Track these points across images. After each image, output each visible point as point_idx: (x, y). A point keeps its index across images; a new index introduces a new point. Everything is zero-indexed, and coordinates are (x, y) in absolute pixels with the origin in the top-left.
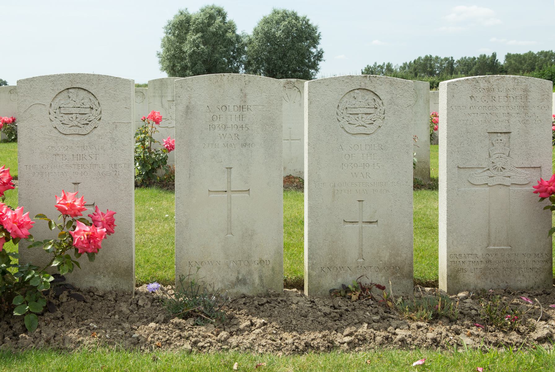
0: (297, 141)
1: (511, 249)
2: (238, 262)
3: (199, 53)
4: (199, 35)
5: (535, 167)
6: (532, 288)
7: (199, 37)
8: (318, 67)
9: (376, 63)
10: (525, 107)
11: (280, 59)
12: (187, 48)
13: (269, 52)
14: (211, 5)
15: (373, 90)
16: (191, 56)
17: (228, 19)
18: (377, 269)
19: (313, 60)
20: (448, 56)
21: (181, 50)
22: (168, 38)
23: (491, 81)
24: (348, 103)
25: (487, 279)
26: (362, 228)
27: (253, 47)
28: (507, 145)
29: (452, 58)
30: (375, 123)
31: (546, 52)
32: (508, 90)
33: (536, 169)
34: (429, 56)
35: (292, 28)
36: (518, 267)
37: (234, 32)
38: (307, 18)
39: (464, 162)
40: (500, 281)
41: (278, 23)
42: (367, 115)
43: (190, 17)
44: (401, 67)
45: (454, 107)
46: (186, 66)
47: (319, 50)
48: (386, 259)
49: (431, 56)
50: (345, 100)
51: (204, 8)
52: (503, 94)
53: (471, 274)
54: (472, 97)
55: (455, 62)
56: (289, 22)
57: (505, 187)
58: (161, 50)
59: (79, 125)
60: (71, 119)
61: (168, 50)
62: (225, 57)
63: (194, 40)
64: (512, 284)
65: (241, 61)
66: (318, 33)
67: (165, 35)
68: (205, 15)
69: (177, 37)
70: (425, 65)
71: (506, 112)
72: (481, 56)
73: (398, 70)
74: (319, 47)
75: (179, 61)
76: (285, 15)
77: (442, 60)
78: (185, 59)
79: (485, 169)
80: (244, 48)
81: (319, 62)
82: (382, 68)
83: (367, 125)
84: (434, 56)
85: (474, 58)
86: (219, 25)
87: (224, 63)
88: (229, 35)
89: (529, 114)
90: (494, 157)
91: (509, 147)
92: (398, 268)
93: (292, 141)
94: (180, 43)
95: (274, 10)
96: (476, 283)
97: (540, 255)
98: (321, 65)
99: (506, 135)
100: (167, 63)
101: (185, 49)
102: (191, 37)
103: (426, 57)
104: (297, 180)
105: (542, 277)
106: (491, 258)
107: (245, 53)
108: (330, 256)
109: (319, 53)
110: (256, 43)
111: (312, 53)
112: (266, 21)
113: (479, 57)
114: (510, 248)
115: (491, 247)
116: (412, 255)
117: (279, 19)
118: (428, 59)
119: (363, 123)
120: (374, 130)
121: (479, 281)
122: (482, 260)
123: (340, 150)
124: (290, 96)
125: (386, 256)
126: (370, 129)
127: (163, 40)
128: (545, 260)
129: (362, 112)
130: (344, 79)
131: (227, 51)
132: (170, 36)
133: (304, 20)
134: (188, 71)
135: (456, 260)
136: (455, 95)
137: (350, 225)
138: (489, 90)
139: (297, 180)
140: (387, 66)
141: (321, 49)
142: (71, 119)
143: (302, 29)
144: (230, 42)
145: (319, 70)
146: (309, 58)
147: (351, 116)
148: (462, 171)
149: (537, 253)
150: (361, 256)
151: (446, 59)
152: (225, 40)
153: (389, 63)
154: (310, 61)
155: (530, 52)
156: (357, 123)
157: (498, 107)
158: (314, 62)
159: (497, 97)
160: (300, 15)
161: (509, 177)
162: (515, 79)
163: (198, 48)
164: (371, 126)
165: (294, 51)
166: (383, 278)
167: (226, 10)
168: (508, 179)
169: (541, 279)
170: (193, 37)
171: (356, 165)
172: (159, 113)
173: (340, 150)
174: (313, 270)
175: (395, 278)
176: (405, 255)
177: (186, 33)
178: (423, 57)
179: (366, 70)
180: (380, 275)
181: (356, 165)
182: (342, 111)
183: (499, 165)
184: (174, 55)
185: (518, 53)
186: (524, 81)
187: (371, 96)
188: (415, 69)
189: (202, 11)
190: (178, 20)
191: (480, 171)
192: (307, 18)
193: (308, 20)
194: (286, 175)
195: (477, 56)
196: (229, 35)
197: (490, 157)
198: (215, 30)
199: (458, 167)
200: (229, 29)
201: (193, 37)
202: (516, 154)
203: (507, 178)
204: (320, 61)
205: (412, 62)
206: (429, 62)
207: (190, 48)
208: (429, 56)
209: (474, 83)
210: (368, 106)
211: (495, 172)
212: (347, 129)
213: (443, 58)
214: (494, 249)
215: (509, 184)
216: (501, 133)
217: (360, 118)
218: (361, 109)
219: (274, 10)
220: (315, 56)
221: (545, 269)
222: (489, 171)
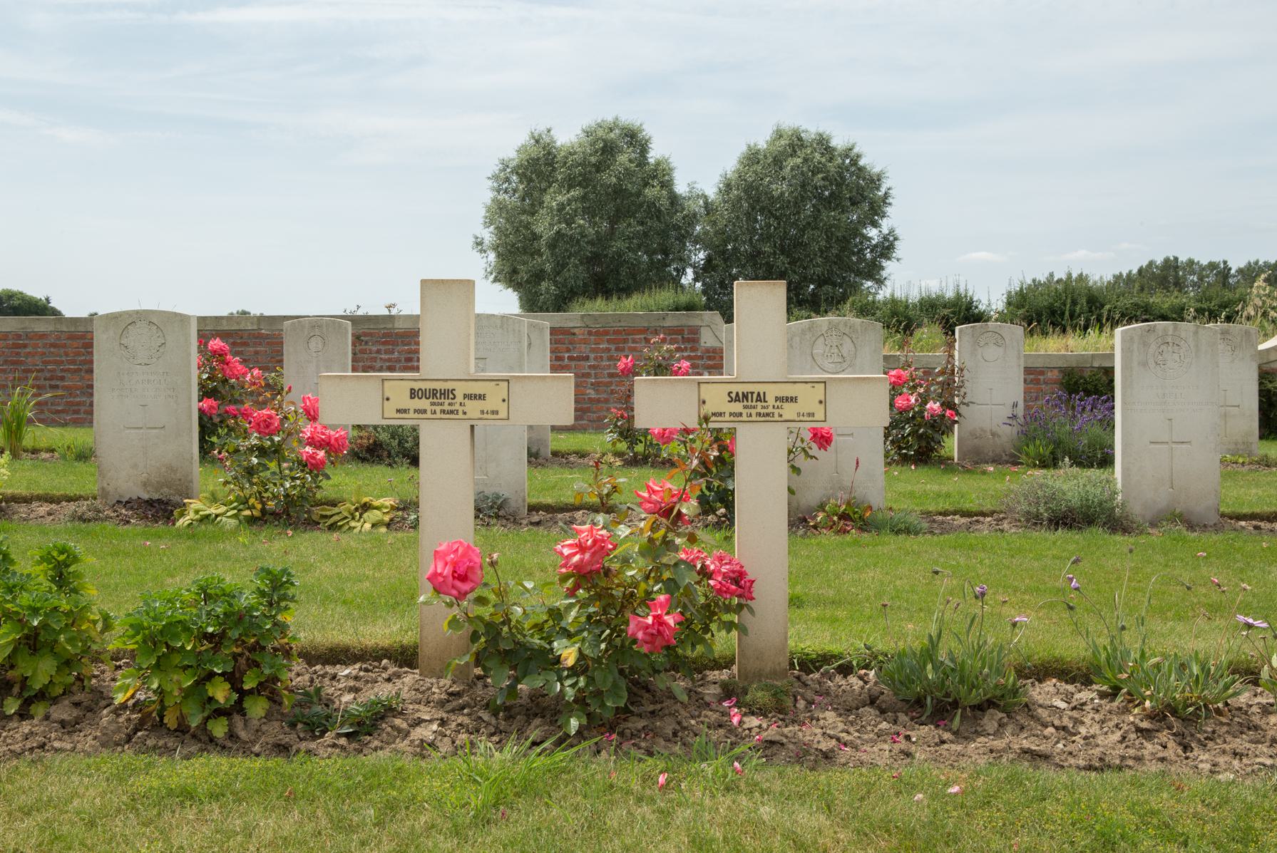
3: (571, 237)
8: (884, 274)
9: (1052, 275)
12: (544, 226)
14: (610, 118)
16: (552, 245)
17: (653, 155)
20: (1216, 259)
29: (1225, 262)
35: (813, 174)
38: (855, 151)
46: (542, 271)
47: (885, 231)
49: (1176, 259)
55: (1233, 272)
56: (806, 160)
58: (488, 235)
63: (561, 207)
66: (883, 190)
74: (885, 225)
76: (796, 143)
77: (1203, 269)
81: (885, 263)
84: (1183, 258)
86: (626, 169)
98: (890, 268)
102: (555, 198)
103: (1167, 260)
110: (724, 214)
111: (869, 239)
112: (752, 158)
117: (782, 153)
118: (1171, 265)
131: (645, 234)
141: (891, 231)
144: (654, 211)
145: (887, 282)
146: (861, 251)
151: (1212, 266)
158: (874, 260)
160: (838, 142)
165: (816, 233)
167: (649, 130)
170: (559, 198)
178: (1159, 260)
192: (855, 151)
193: (859, 156)
198: (614, 180)
200: (655, 177)
201: (559, 198)
204: (889, 259)
205: (1135, 271)
207: (551, 225)
213: (1204, 262)
220: (876, 246)
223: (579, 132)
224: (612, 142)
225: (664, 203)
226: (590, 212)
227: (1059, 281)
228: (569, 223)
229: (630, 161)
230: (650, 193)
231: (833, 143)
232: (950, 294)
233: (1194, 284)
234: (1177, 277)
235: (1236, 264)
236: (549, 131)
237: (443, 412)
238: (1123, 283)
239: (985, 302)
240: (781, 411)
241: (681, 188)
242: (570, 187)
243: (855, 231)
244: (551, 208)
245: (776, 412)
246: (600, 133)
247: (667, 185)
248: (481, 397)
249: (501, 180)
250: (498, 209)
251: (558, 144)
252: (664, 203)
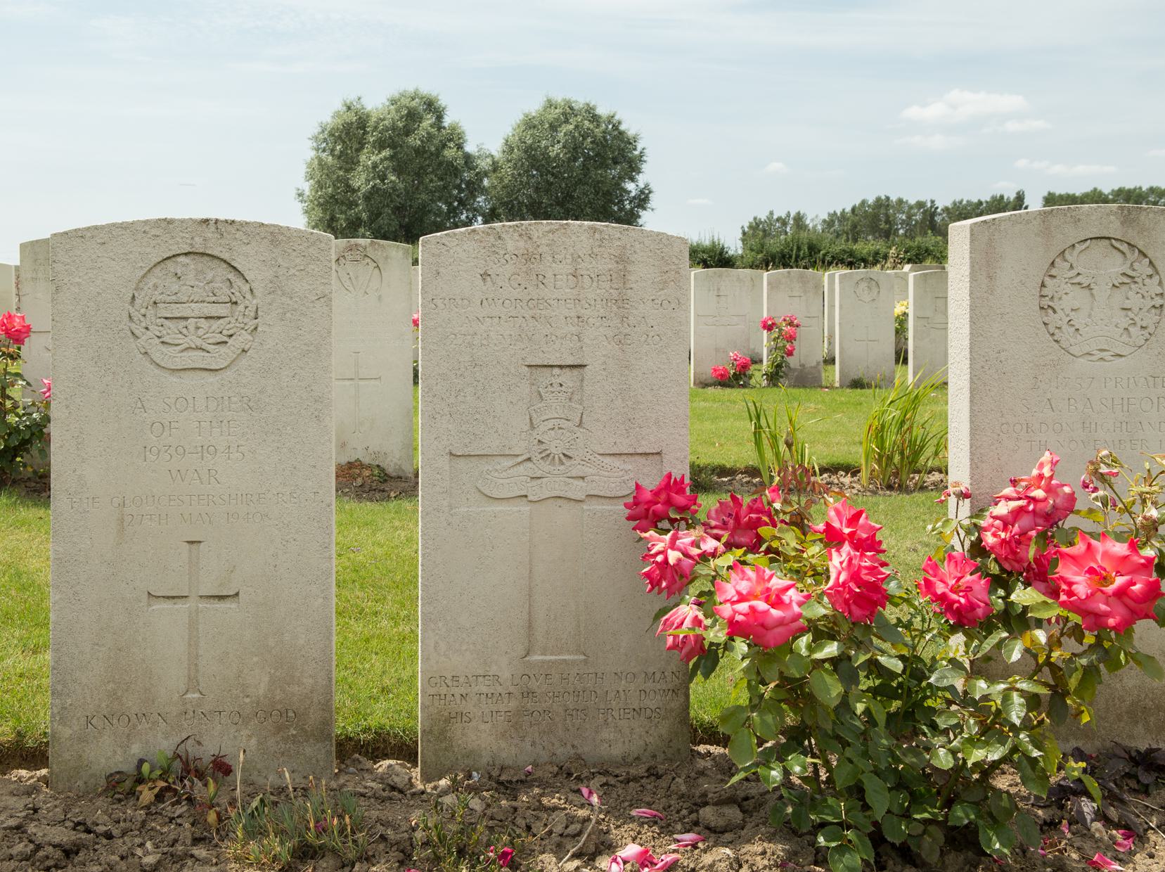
0: (372, 382)
1: (586, 662)
3: (385, 192)
4: (386, 153)
5: (646, 454)
6: (638, 758)
7: (386, 159)
9: (771, 213)
10: (621, 301)
11: (558, 204)
12: (360, 181)
13: (537, 189)
14: (411, 89)
15: (226, 256)
16: (368, 198)
17: (447, 121)
18: (236, 719)
19: (628, 207)
20: (923, 199)
21: (348, 186)
22: (320, 160)
23: (535, 235)
24: (160, 290)
25: (523, 739)
26: (197, 611)
27: (501, 179)
28: (576, 397)
29: (933, 202)
30: (231, 341)
31: (1129, 191)
32: (576, 258)
33: (651, 457)
35: (584, 139)
36: (602, 706)
37: (460, 147)
38: (617, 118)
39: (467, 441)
40: (557, 744)
41: (553, 127)
42: (212, 321)
43: (368, 116)
44: (824, 221)
45: (439, 302)
46: (359, 219)
47: (642, 185)
48: (261, 692)
49: (888, 198)
50: (152, 280)
51: (397, 95)
52: (565, 268)
53: (483, 727)
54: (485, 276)
56: (577, 127)
57: (572, 503)
58: (307, 187)
59: (205, 346)
60: (184, 331)
61: (320, 185)
62: (440, 199)
63: (375, 166)
64: (586, 749)
65: (475, 210)
67: (313, 153)
68: (398, 111)
69: (339, 157)
70: (875, 217)
71: (573, 314)
73: (819, 227)
74: (642, 179)
75: (344, 208)
76: (569, 112)
77: (911, 207)
78: (357, 205)
79: (520, 459)
80: (481, 181)
81: (642, 213)
82: (784, 223)
83: (210, 348)
87: (439, 213)
88: (449, 153)
89: (632, 320)
90: (543, 428)
91: (581, 402)
92: (291, 714)
93: (361, 383)
94: (347, 171)
95: (549, 101)
96: (494, 748)
97: (658, 676)
99: (576, 372)
100: (319, 213)
101: (356, 183)
102: (369, 158)
103: (878, 199)
104: (367, 473)
105: (664, 729)
106: (534, 685)
107: (484, 191)
108: (111, 685)
110: (507, 170)
112: (530, 124)
114: (582, 657)
115: (537, 657)
116: (330, 679)
117: (557, 120)
118: (882, 204)
119: (199, 342)
120: (229, 361)
121: (503, 745)
122: (511, 689)
123: (137, 411)
124: (357, 277)
125: (260, 683)
126: (220, 357)
127: (310, 165)
128: (670, 686)
129: (197, 313)
130: (147, 228)
131: (445, 187)
132: (324, 155)
133: (609, 122)
134: (362, 230)
135: (444, 690)
136: (441, 270)
137: (167, 605)
138: (529, 258)
139: (367, 473)
140: (795, 219)
141: (647, 186)
142: (184, 331)
143: (606, 141)
144: (452, 170)
146: (621, 201)
147: (166, 322)
148: (462, 463)
149: (651, 670)
150: (193, 683)
151: (920, 205)
152: (440, 164)
153: (799, 213)
154: (621, 210)
155: (1095, 189)
156: (185, 342)
157: (552, 302)
158: (632, 209)
159: (549, 275)
160: (602, 111)
161: (583, 478)
162: (595, 230)
163: (382, 181)
164: (223, 349)
165: (587, 188)
166: (253, 741)
167: (442, 101)
168: (580, 483)
169: (660, 736)
170: (373, 158)
171: (180, 450)
172: (23, 318)
173: (137, 411)
174: (65, 725)
175: (286, 740)
176: (311, 681)
177: (359, 150)
178: (871, 201)
179: (750, 227)
180: (245, 732)
181: (180, 450)
182: (143, 311)
183: (556, 448)
184: (332, 197)
185: (1071, 192)
186: (618, 235)
187: (223, 271)
188: (854, 226)
189: (393, 102)
190: (340, 121)
191: (507, 463)
193: (620, 123)
194: (344, 460)
196: (449, 153)
197: (532, 427)
199: (451, 454)
200: (450, 140)
201: (373, 158)
202: (598, 420)
203: (576, 482)
204: (645, 209)
205: (848, 209)
206: (883, 211)
207: (368, 181)
209: (492, 239)
210: (214, 299)
211: (546, 466)
212: (156, 357)
213: (912, 202)
214: (543, 662)
215: (581, 496)
216: (561, 367)
217: (192, 328)
218: (193, 305)
219: (549, 101)
220: (634, 198)
221: (672, 710)
222: (529, 465)
224: (415, 109)
226: (399, 171)
232: (707, 243)
233: (903, 222)
234: (887, 216)
235: (941, 204)
239: (733, 248)
243: (617, 185)
246: (405, 102)
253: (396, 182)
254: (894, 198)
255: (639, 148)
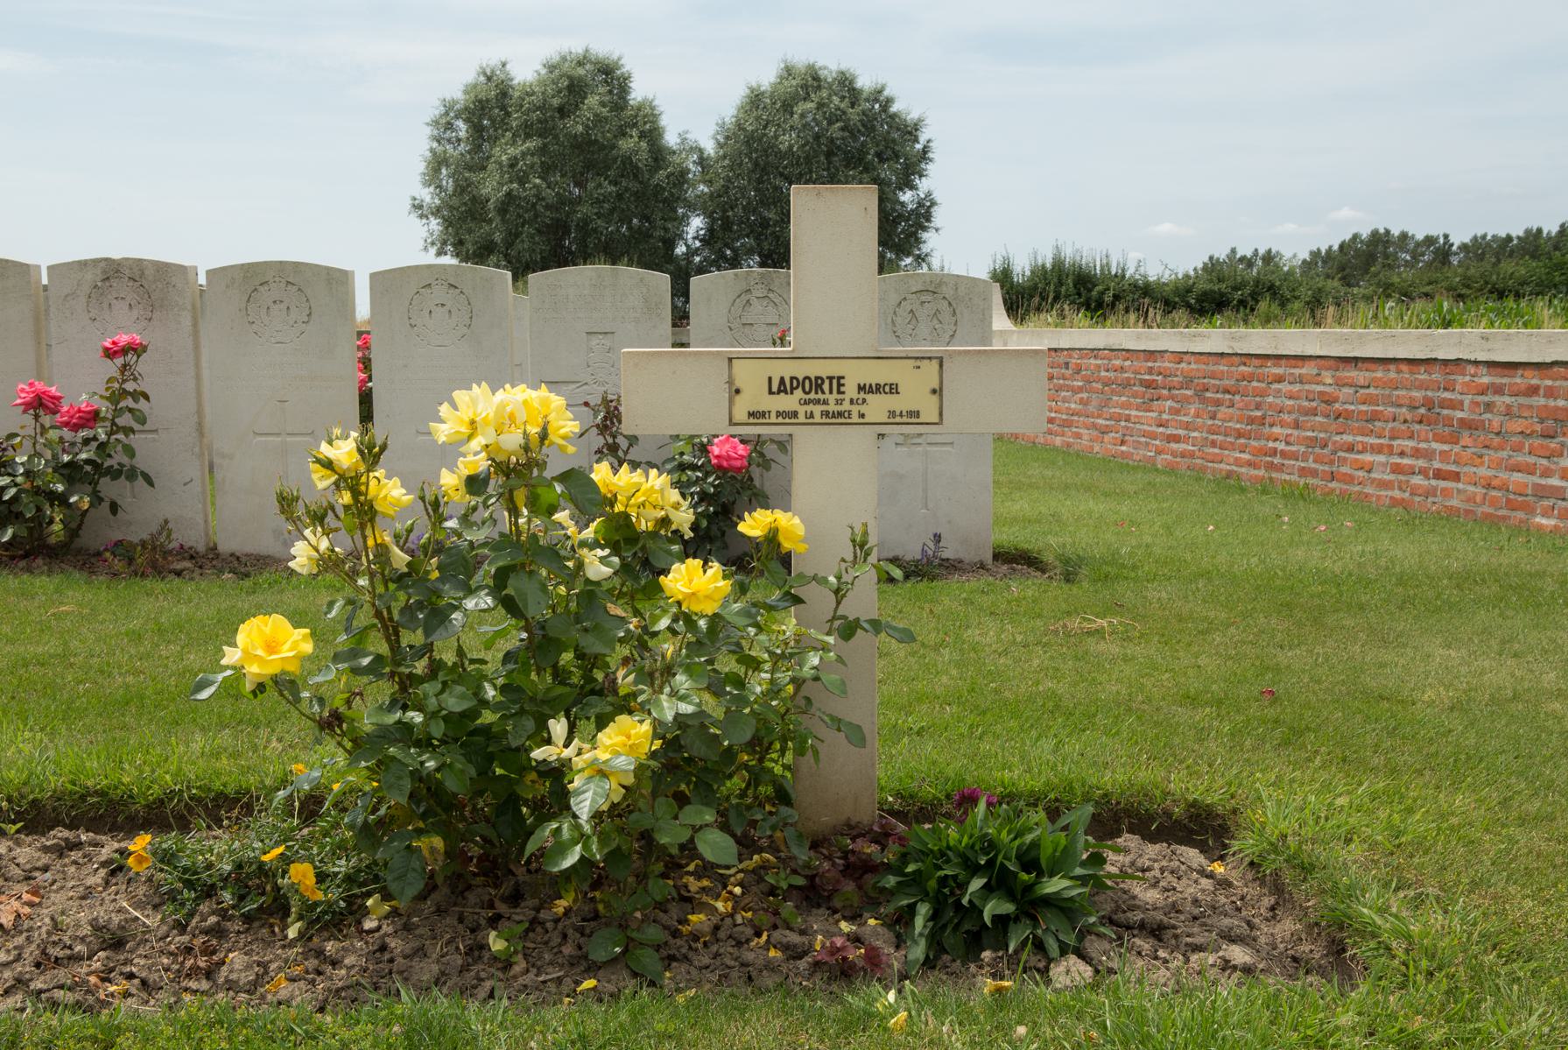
2: (766, 790)
4: (531, 144)
8: (925, 248)
9: (1233, 251)
12: (491, 187)
14: (578, 49)
16: (503, 210)
20: (1433, 233)
29: (1446, 236)
34: (1382, 231)
35: (830, 123)
38: (886, 93)
44: (1304, 261)
49: (1387, 232)
51: (556, 59)
55: (1454, 248)
56: (820, 106)
58: (427, 195)
72: (1528, 232)
74: (924, 185)
76: (811, 81)
85: (1509, 238)
86: (596, 115)
102: (505, 151)
103: (1375, 233)
109: (920, 204)
112: (755, 99)
113: (1521, 234)
131: (620, 196)
133: (876, 100)
141: (929, 194)
144: (628, 167)
151: (1430, 241)
153: (1269, 251)
160: (864, 82)
167: (629, 65)
170: (511, 151)
178: (1365, 233)
189: (551, 68)
193: (889, 101)
195: (1517, 231)
200: (635, 125)
201: (511, 151)
205: (1336, 247)
206: (1380, 248)
208: (1382, 231)
213: (1420, 237)
223: (539, 67)
224: (580, 79)
225: (643, 156)
227: (1242, 259)
228: (522, 181)
229: (603, 104)
230: (626, 145)
231: (859, 84)
236: (504, 65)
237: (826, 414)
238: (1479, 249)
240: (863, 409)
241: (671, 139)
242: (528, 136)
244: (500, 164)
245: (855, 409)
247: (652, 134)
248: (893, 389)
249: (444, 125)
250: (437, 163)
251: (515, 82)
252: (643, 156)
253: (558, 183)
254: (1396, 232)
255: (923, 139)
